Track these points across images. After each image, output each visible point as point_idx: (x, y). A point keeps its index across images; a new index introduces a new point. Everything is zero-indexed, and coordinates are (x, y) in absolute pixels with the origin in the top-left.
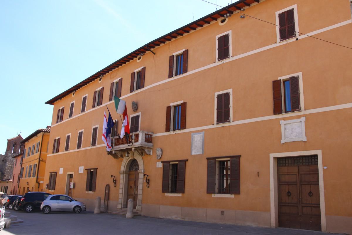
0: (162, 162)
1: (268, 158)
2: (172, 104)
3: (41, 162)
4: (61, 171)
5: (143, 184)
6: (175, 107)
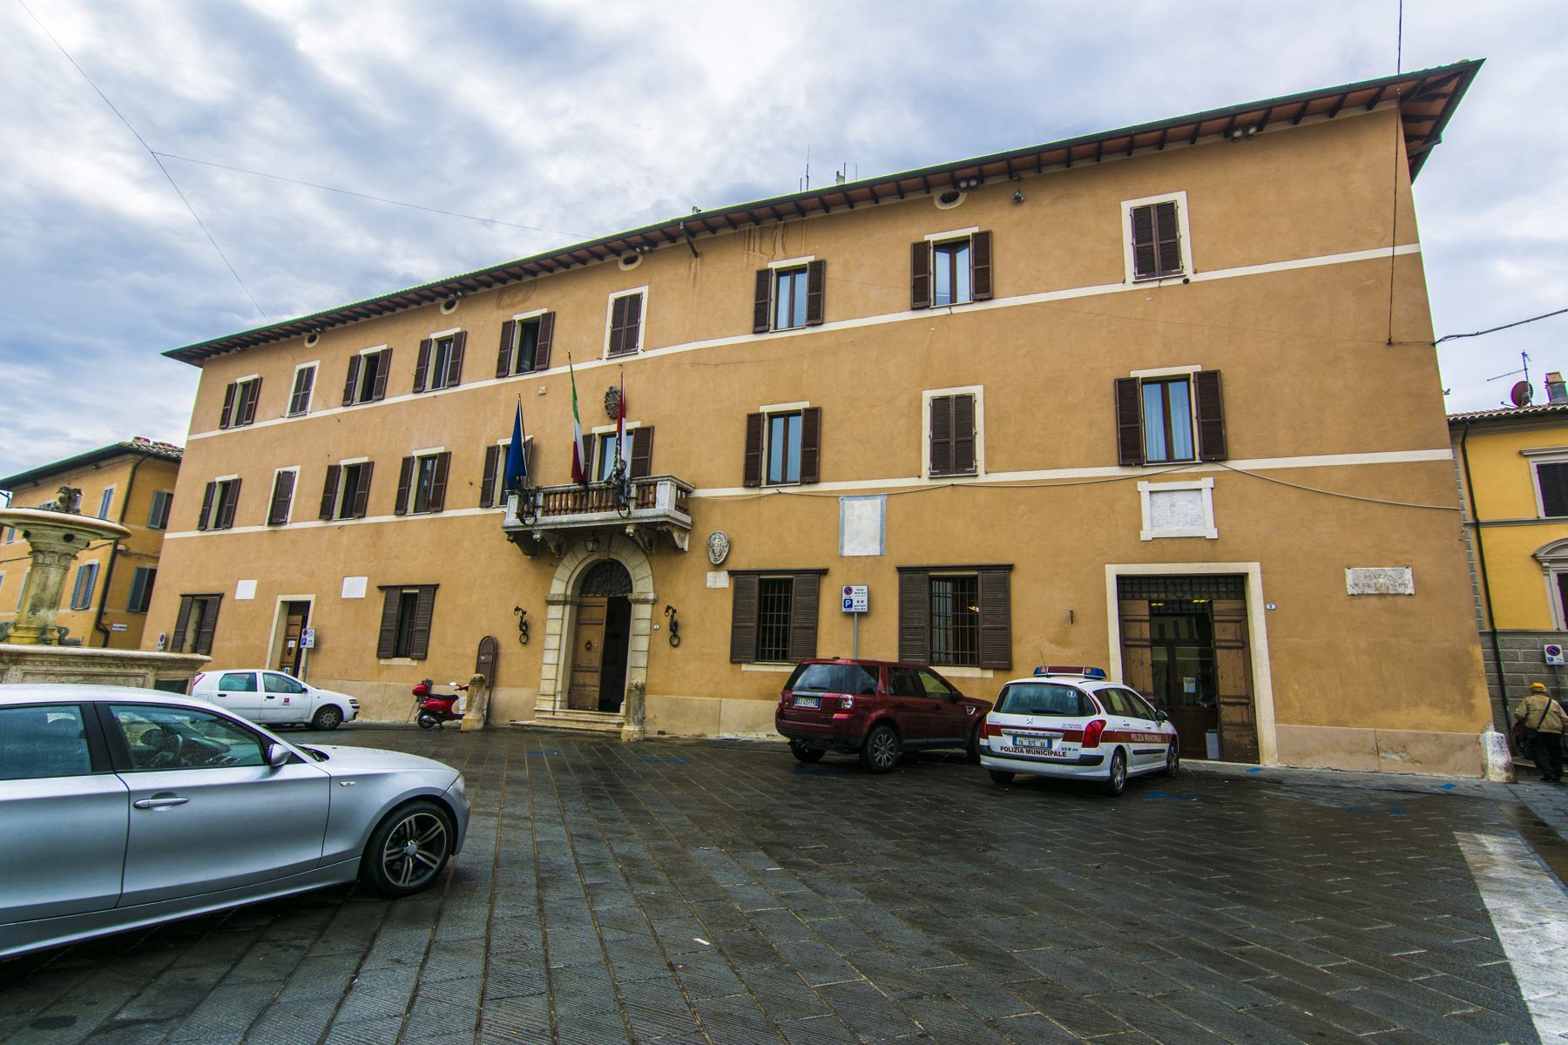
0: (732, 573)
1: (1102, 574)
2: (416, 454)
3: (119, 559)
4: (246, 590)
5: (652, 633)
6: (424, 459)
